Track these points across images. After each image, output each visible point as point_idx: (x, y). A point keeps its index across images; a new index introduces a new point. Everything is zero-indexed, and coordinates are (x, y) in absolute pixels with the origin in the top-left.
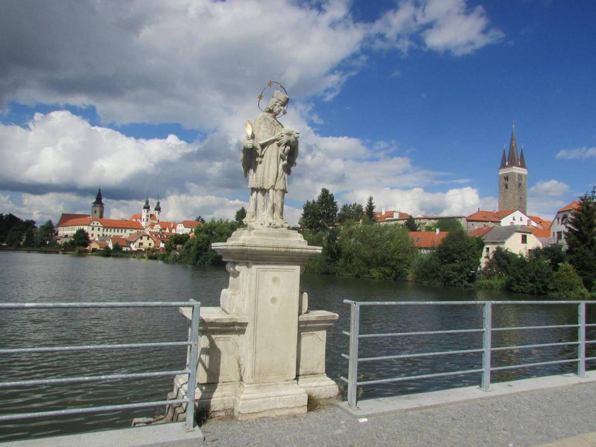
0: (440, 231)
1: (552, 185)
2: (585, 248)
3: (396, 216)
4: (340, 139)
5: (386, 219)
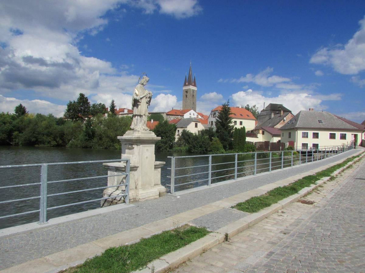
0: (154, 121)
2: (224, 130)
5: (120, 113)
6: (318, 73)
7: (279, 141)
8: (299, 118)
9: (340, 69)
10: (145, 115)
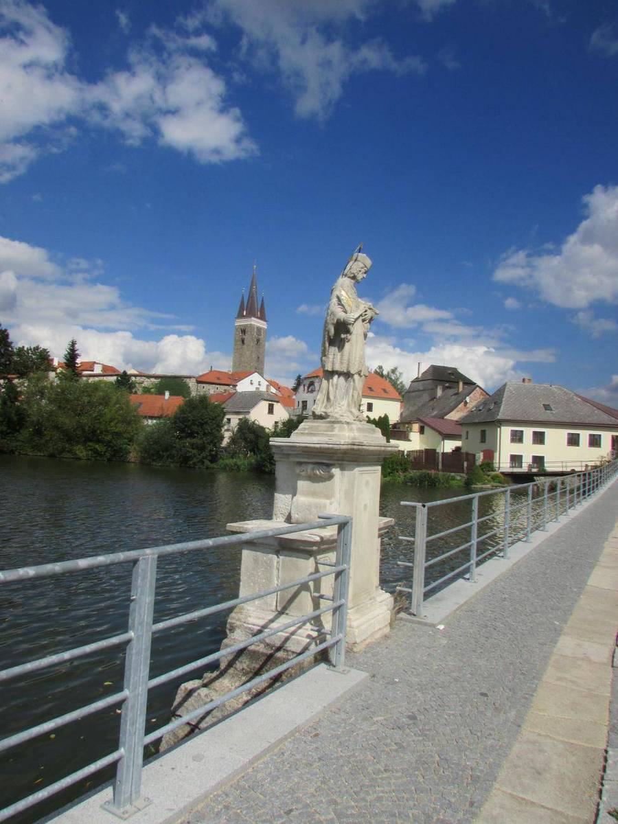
0: (170, 395)
1: (287, 342)
3: (98, 370)
4: (16, 243)
6: (511, 303)
7: (458, 449)
8: (504, 399)
9: (555, 294)
10: (359, 374)
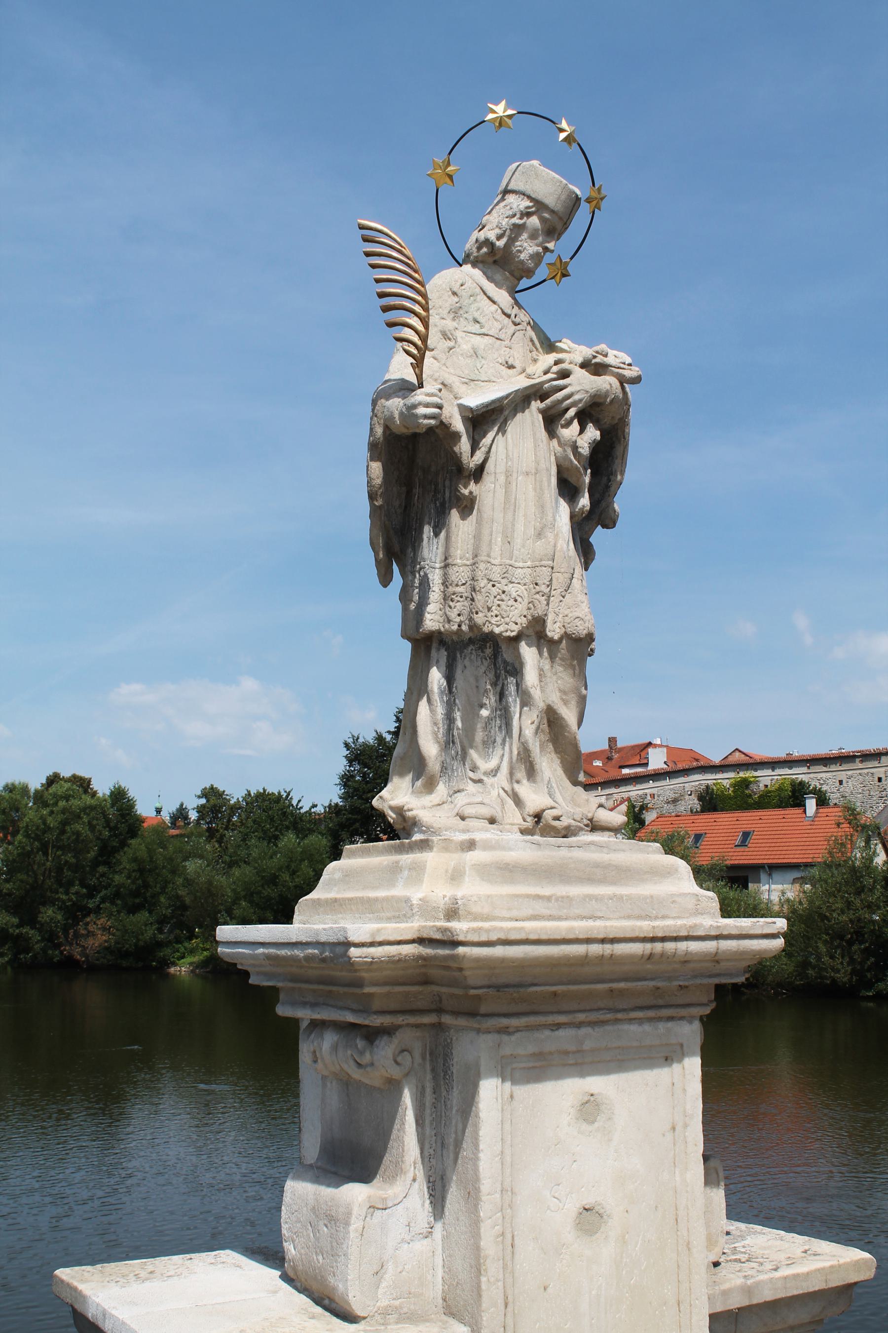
3: (657, 760)
